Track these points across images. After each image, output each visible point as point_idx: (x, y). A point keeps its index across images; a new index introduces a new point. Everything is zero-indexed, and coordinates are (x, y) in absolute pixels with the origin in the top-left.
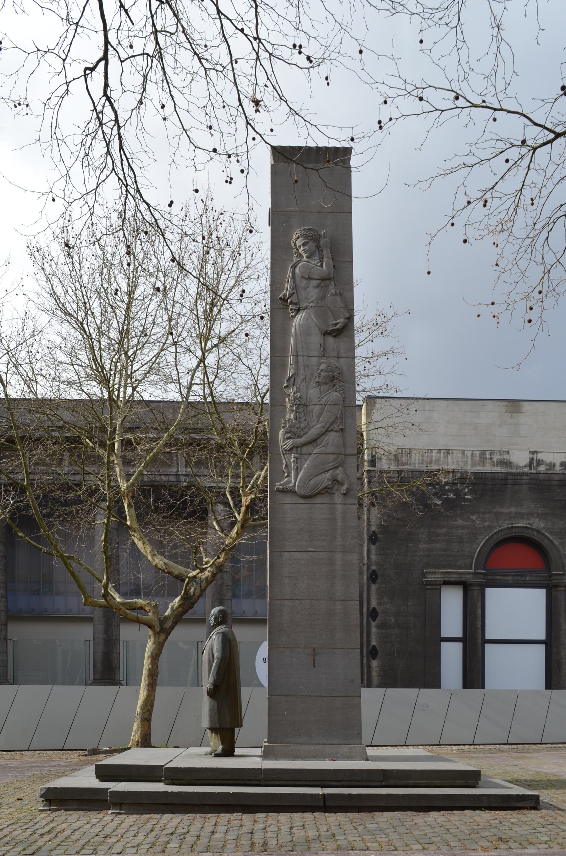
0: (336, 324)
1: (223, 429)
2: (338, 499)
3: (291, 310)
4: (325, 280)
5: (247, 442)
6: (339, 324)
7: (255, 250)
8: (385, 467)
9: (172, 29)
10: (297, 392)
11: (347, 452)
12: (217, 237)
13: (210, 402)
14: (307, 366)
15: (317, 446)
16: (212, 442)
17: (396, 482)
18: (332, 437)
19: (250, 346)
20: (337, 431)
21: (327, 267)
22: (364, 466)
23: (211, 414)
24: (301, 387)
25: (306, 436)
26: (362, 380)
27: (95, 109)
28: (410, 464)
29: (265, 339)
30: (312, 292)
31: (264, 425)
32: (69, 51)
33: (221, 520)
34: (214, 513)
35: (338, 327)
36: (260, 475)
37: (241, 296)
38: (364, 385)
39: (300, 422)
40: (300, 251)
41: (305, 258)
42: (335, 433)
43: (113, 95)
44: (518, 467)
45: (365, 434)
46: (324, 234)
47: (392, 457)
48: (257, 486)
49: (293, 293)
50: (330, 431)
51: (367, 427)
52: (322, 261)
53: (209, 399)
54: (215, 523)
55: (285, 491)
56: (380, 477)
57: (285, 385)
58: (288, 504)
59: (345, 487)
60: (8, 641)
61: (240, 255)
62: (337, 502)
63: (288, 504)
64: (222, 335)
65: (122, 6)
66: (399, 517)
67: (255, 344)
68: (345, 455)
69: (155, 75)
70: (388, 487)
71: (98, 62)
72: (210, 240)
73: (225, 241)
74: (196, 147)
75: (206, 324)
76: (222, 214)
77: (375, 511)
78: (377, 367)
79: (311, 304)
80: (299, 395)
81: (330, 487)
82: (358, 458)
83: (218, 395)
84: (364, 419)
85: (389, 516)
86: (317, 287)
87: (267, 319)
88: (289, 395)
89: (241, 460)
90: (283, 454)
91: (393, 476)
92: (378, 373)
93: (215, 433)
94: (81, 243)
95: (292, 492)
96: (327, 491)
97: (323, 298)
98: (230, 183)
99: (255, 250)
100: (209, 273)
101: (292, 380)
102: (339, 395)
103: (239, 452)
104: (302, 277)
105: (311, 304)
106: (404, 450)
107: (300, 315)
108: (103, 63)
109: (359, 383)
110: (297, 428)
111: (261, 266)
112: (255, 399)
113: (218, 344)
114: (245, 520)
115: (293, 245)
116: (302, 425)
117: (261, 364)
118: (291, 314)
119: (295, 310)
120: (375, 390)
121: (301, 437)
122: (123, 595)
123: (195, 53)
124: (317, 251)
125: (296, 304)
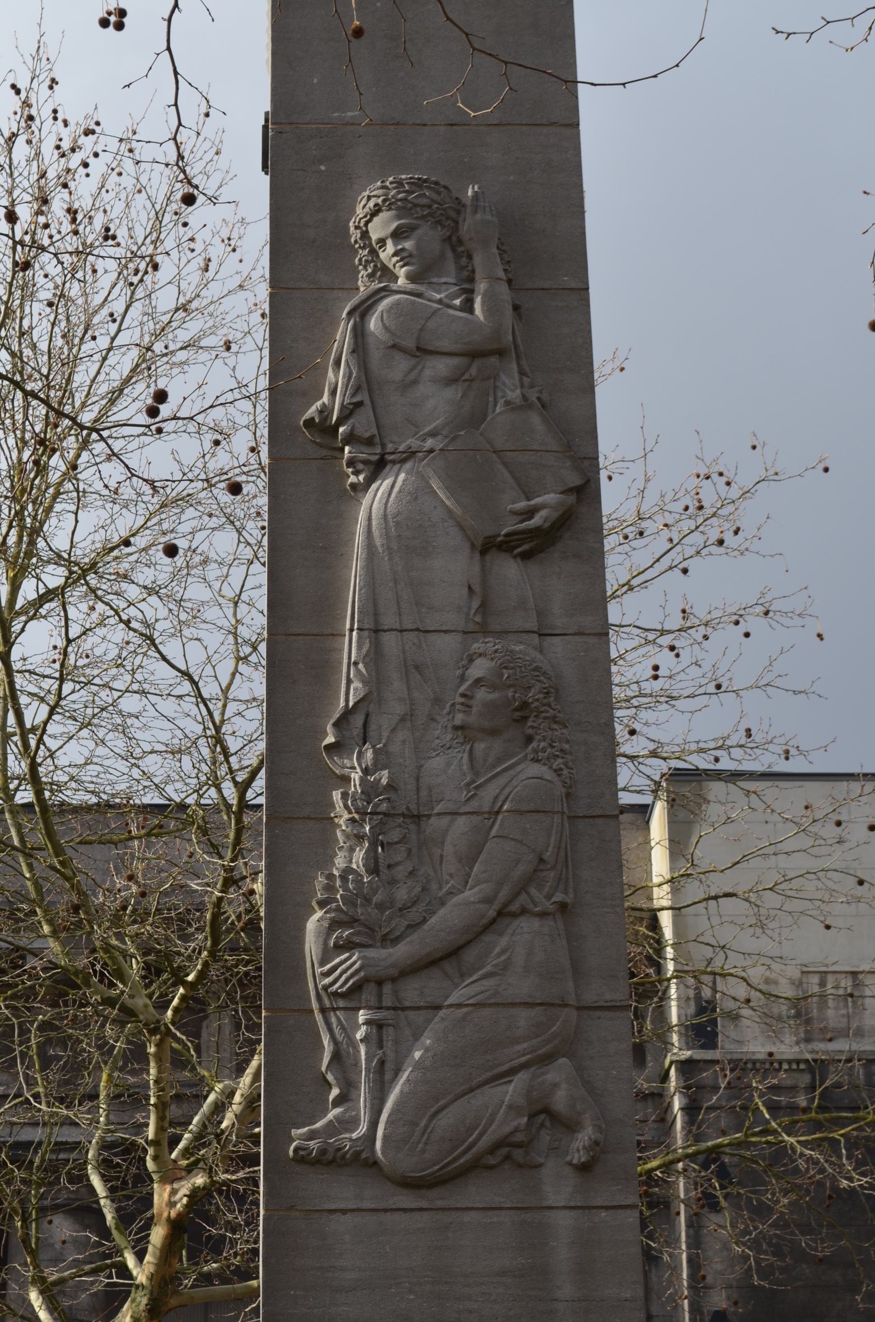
0: (530, 513)
1: (76, 909)
2: (557, 1187)
3: (351, 463)
4: (481, 356)
5: (178, 961)
6: (543, 513)
7: (217, 251)
8: (757, 1047)
10: (377, 766)
11: (590, 997)
12: (69, 211)
13: (28, 806)
14: (417, 667)
15: (463, 976)
16: (32, 962)
17: (805, 1110)
18: (524, 937)
19: (196, 591)
20: (543, 915)
21: (491, 308)
22: (667, 1045)
23: (28, 856)
24: (394, 748)
25: (415, 937)
26: (644, 715)
28: (860, 1033)
29: (257, 567)
30: (435, 401)
31: (252, 892)
33: (62, 1281)
34: (33, 1253)
35: (537, 521)
36: (232, 1094)
37: (153, 412)
38: (653, 732)
39: (393, 882)
40: (383, 255)
41: (401, 281)
42: (536, 923)
45: (666, 919)
46: (476, 194)
47: (783, 1009)
48: (218, 1136)
49: (359, 404)
50: (514, 915)
51: (675, 891)
52: (472, 291)
53: (24, 796)
54: (35, 1297)
55: (328, 1160)
56: (737, 1088)
57: (330, 739)
58: (344, 1212)
59: (585, 1136)
61: (156, 267)
62: (549, 1203)
63: (344, 1212)
64: (84, 552)
66: (824, 1250)
67: (216, 585)
68: (580, 1009)
70: (774, 1132)
72: (42, 220)
73: (99, 221)
75: (19, 514)
76: (88, 132)
77: (721, 1226)
78: (707, 666)
79: (429, 443)
80: (384, 777)
81: (519, 1137)
82: (639, 1015)
83: (61, 777)
84: (660, 864)
85: (778, 1253)
86: (451, 381)
87: (258, 494)
88: (346, 779)
89: (153, 1032)
90: (323, 1010)
91: (789, 1083)
92: (711, 688)
93: (46, 929)
95: (361, 1161)
96: (509, 1155)
97: (475, 419)
98: (119, 26)
99: (217, 251)
100: (36, 334)
101: (358, 720)
102: (549, 775)
103: (141, 1002)
104: (394, 346)
105: (429, 443)
106: (830, 979)
107: (388, 482)
109: (637, 726)
110: (381, 907)
111: (239, 303)
112: (213, 792)
113: (64, 588)
114: (164, 1282)
116: (402, 894)
117: (239, 659)
118: (353, 479)
119: (365, 462)
120: (701, 751)
121: (396, 941)
124: (449, 254)
125: (369, 442)
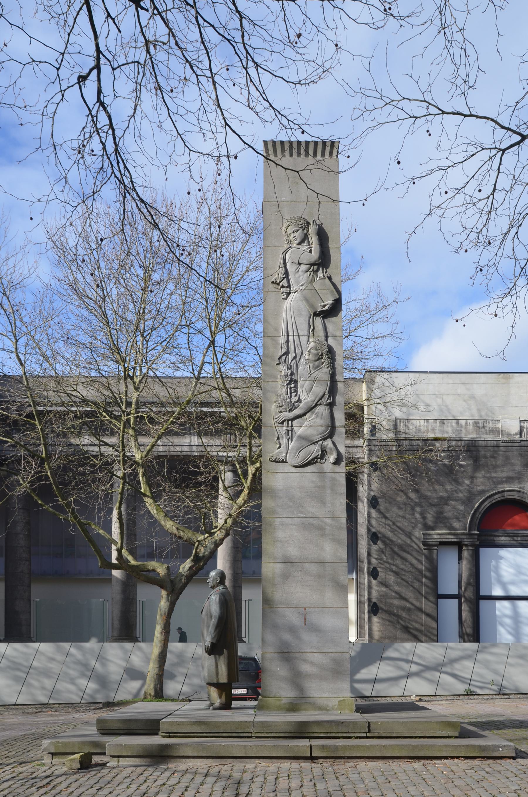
0: (324, 306)
9: (165, 39)
27: (91, 113)
32: (62, 61)
35: (326, 308)
43: (107, 101)
44: (509, 434)
60: (32, 602)
65: (109, 15)
69: (149, 82)
71: (91, 70)
79: (301, 288)
94: (182, 254)
105: (301, 288)
108: (95, 72)
115: (284, 232)
122: (135, 558)
123: (187, 61)
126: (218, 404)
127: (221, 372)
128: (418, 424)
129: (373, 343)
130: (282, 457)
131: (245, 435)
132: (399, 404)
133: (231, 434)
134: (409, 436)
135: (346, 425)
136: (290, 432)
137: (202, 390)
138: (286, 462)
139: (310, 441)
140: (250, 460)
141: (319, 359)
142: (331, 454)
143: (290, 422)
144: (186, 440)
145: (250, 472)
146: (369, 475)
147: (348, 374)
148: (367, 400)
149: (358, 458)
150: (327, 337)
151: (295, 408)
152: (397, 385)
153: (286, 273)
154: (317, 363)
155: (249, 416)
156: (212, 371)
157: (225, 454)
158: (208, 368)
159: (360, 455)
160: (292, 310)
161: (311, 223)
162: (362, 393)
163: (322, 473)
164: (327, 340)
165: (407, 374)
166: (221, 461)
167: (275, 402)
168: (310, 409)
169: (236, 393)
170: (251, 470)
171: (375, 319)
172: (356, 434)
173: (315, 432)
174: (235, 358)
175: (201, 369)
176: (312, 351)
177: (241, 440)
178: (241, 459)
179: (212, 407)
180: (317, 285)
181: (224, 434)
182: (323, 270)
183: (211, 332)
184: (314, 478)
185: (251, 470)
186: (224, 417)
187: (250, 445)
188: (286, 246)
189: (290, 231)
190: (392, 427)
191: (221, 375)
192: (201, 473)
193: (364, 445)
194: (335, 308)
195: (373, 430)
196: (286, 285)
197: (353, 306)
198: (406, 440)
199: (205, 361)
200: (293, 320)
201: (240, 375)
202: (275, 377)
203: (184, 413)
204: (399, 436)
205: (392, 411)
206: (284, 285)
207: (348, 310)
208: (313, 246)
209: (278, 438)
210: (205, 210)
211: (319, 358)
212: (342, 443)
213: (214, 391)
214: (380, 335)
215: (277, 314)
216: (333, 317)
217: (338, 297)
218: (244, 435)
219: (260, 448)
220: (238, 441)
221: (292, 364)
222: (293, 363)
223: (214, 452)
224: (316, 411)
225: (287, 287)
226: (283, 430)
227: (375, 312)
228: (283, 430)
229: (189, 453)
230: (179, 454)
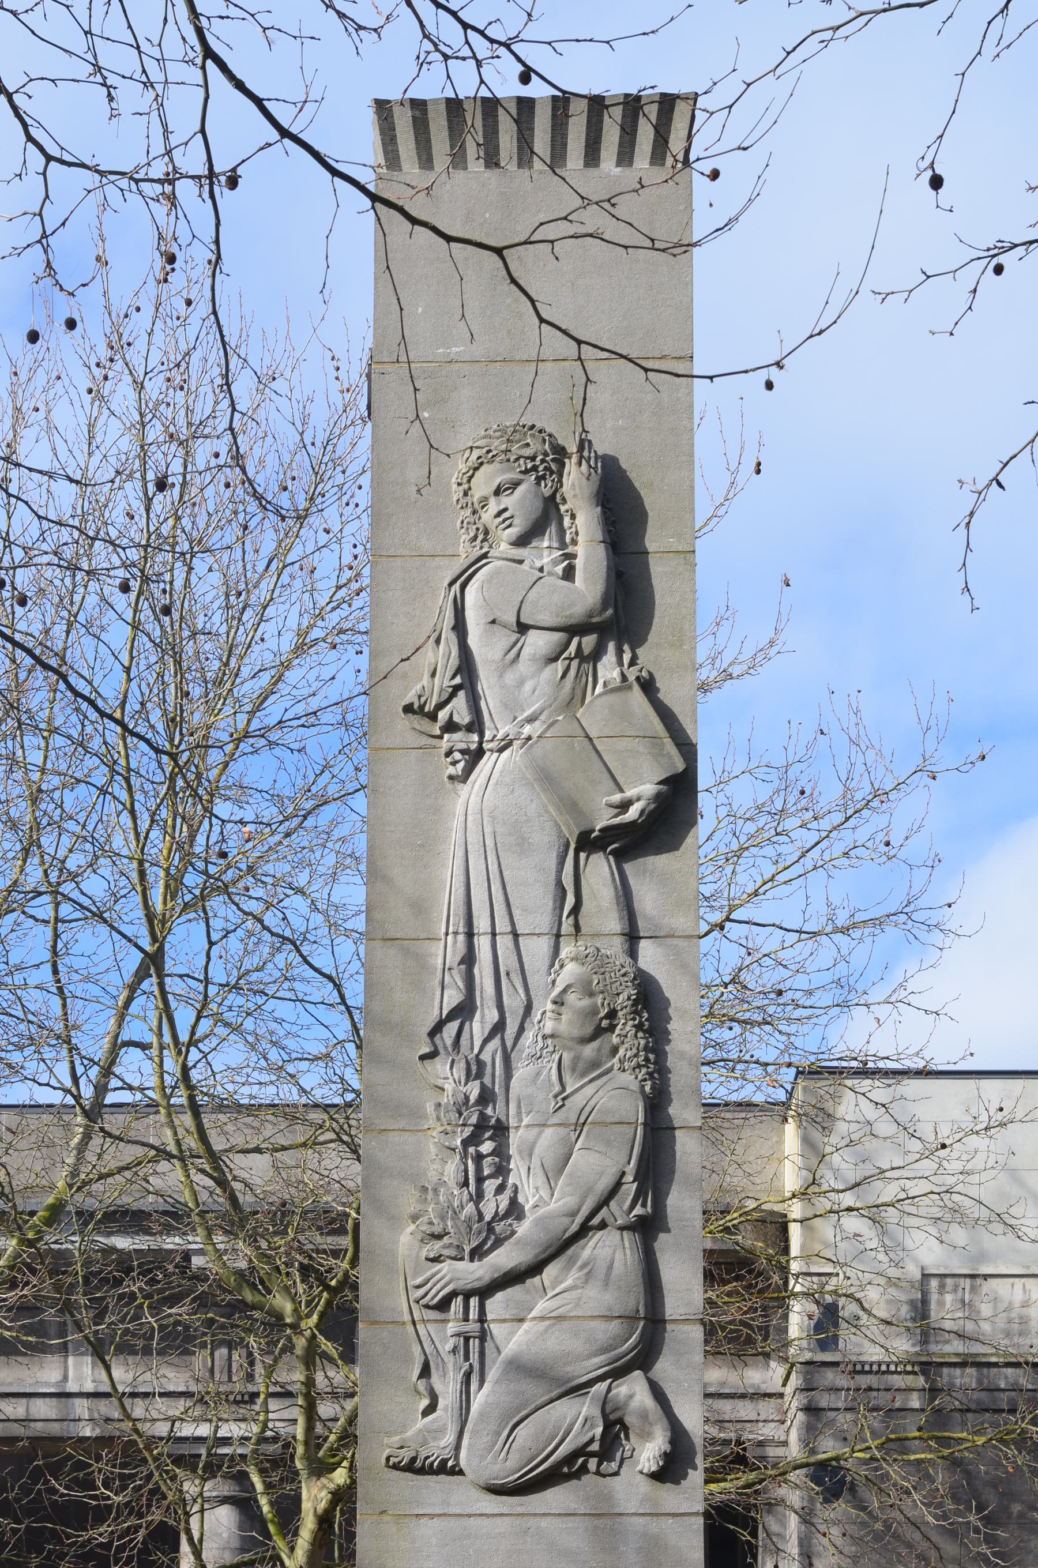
0: (624, 806)
35: (633, 813)
58: (432, 1516)
63: (432, 1516)
74: (49, 158)
79: (527, 730)
105: (527, 730)
115: (456, 493)
126: (175, 1218)
127: (190, 1087)
128: (1018, 1296)
129: (826, 951)
130: (440, 1447)
131: (289, 1348)
132: (936, 1212)
133: (231, 1346)
134: (977, 1348)
135: (710, 1302)
136: (474, 1345)
137: (111, 1163)
138: (461, 1472)
139: (556, 1381)
140: (308, 1457)
141: (599, 1032)
142: (646, 1436)
143: (474, 1302)
144: (46, 1373)
145: (306, 1505)
146: (807, 1518)
147: (717, 1087)
148: (802, 1194)
149: (761, 1444)
150: (632, 937)
151: (499, 1243)
152: (926, 1131)
153: (466, 666)
154: (589, 1050)
155: (305, 1271)
156: (152, 1081)
157: (204, 1430)
158: (134, 1067)
159: (768, 1431)
160: (488, 825)
161: (572, 448)
162: (781, 1164)
163: (604, 1517)
164: (633, 953)
165: (971, 1083)
166: (188, 1462)
167: (414, 1218)
168: (561, 1247)
169: (254, 1171)
170: (314, 1497)
171: (838, 849)
172: (750, 1341)
173: (578, 1346)
174: (249, 1024)
175: (107, 1072)
176: (571, 998)
177: (270, 1370)
178: (271, 1448)
179: (148, 1232)
180: (595, 715)
181: (203, 1345)
182: (620, 653)
183: (150, 917)
184: (574, 1536)
185: (314, 1497)
186: (200, 1276)
187: (307, 1396)
188: (465, 552)
189: (483, 484)
190: (905, 1311)
191: (191, 1098)
192: (101, 1514)
193: (789, 1390)
194: (671, 813)
195: (828, 1321)
196: (463, 717)
197: (745, 794)
198: (963, 1365)
199: (125, 1036)
200: (493, 868)
201: (268, 1094)
202: (416, 1113)
203: (37, 1259)
204: (933, 1348)
205: (909, 1244)
206: (455, 719)
207: (723, 811)
208: (580, 550)
209: (425, 1372)
210: (122, 395)
211: (601, 1029)
212: (690, 1378)
213: (163, 1166)
214: (860, 917)
215: (425, 844)
216: (659, 851)
217: (680, 766)
218: (283, 1350)
219: (349, 1404)
220: (259, 1379)
221: (486, 1057)
222: (492, 1052)
223: (157, 1419)
224: (586, 1253)
225: (469, 728)
226: (445, 1334)
227: (838, 818)
228: (445, 1334)
229: (55, 1429)
230: (17, 1430)
